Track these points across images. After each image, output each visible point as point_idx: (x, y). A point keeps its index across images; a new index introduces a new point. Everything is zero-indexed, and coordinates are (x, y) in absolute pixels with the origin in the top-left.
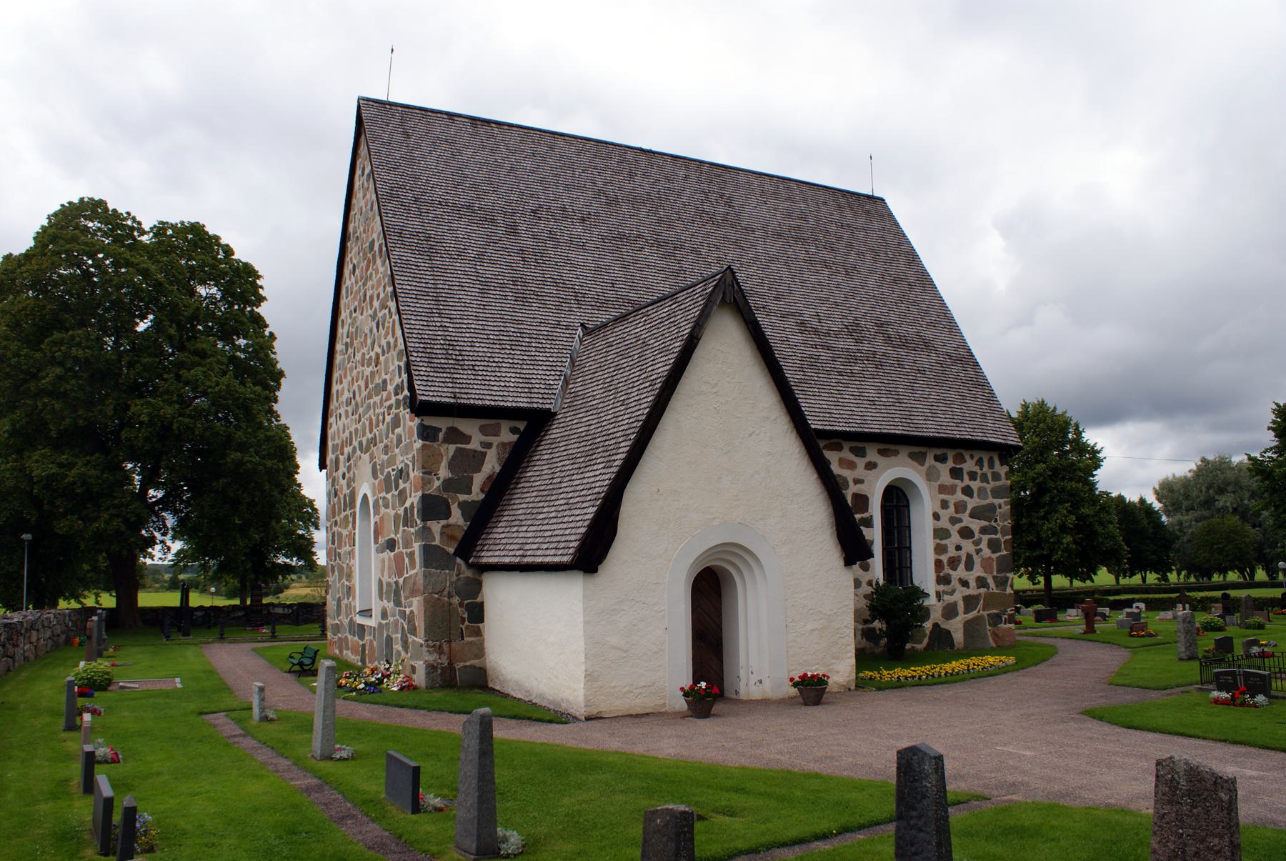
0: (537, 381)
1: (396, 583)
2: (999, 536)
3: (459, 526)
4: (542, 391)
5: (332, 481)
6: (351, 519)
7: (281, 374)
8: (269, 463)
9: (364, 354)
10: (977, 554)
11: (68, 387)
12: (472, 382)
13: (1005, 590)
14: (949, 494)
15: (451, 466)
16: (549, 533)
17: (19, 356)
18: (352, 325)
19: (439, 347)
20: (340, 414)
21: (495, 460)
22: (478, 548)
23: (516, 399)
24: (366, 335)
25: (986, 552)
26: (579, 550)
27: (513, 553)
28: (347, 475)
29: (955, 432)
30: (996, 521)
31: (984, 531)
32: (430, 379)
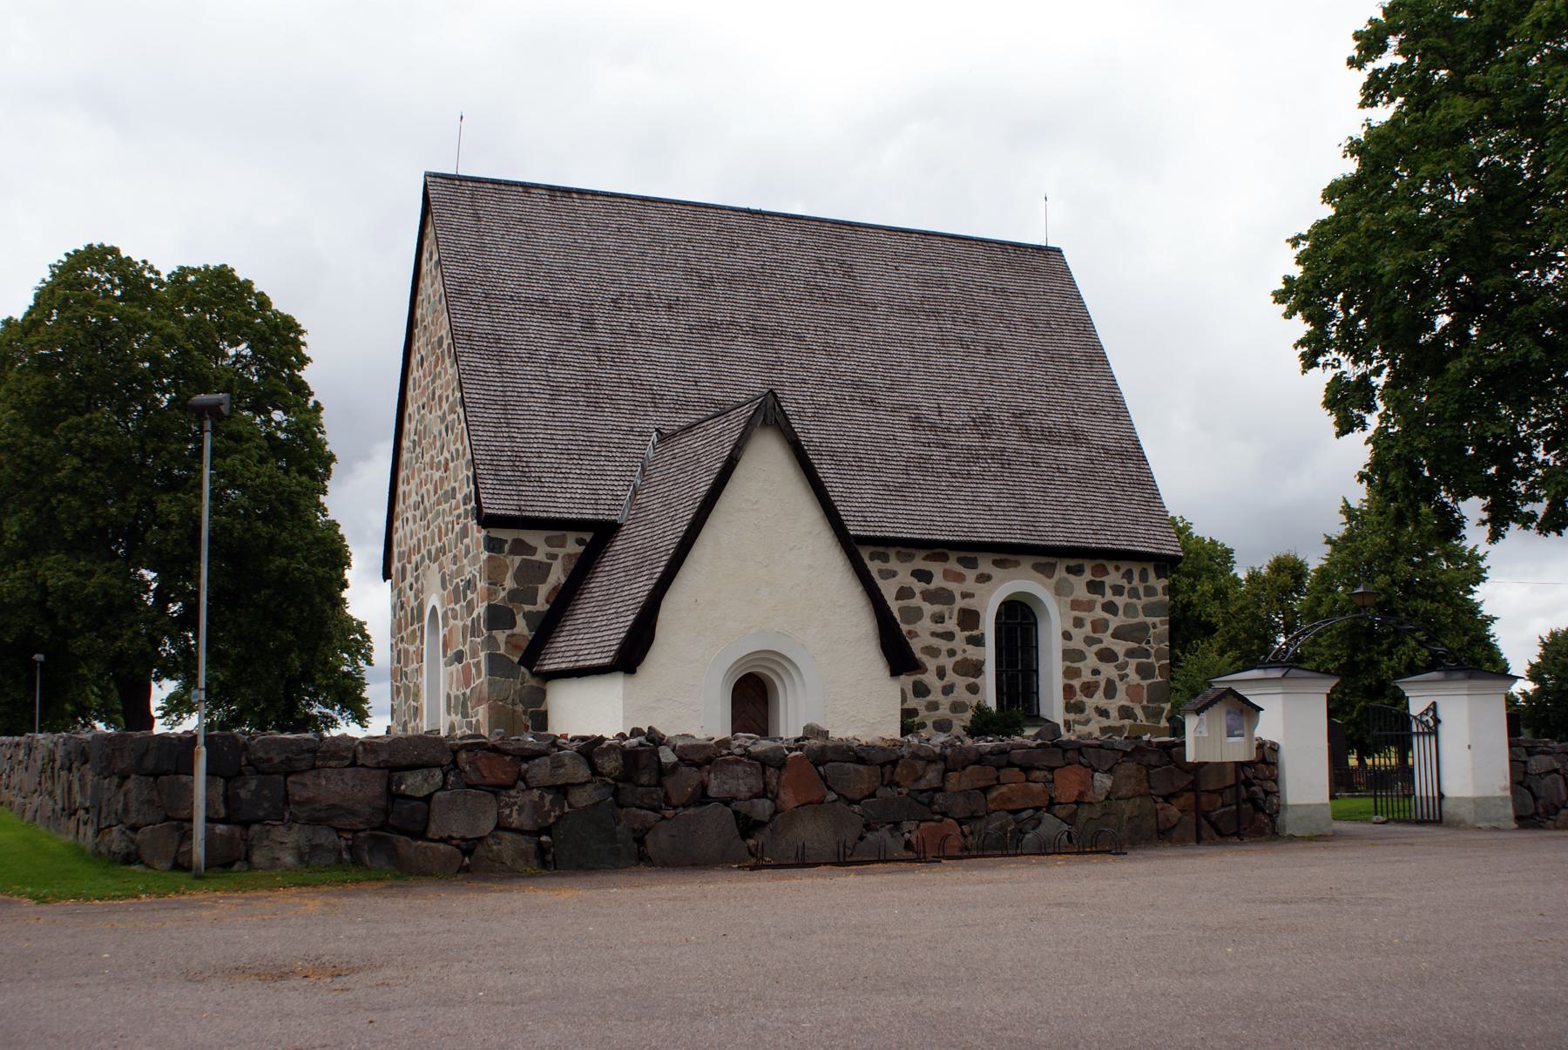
0: (605, 492)
1: (464, 694)
2: (1152, 660)
3: (524, 636)
4: (609, 502)
5: (398, 592)
6: (418, 634)
7: (331, 458)
8: (320, 571)
9: (432, 457)
10: (1121, 680)
11: (87, 481)
12: (537, 494)
13: (1159, 722)
14: (1085, 610)
15: (516, 577)
16: (599, 640)
17: (31, 445)
18: (421, 421)
19: (506, 458)
20: (407, 519)
21: (560, 570)
22: (542, 657)
23: (581, 511)
24: (435, 437)
25: (1134, 678)
26: (619, 652)
27: (568, 659)
28: (415, 585)
29: (1090, 541)
30: (1148, 642)
31: (1130, 653)
32: (496, 492)
